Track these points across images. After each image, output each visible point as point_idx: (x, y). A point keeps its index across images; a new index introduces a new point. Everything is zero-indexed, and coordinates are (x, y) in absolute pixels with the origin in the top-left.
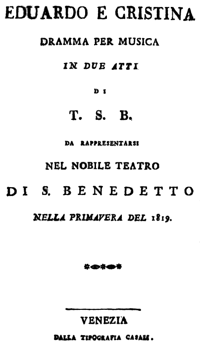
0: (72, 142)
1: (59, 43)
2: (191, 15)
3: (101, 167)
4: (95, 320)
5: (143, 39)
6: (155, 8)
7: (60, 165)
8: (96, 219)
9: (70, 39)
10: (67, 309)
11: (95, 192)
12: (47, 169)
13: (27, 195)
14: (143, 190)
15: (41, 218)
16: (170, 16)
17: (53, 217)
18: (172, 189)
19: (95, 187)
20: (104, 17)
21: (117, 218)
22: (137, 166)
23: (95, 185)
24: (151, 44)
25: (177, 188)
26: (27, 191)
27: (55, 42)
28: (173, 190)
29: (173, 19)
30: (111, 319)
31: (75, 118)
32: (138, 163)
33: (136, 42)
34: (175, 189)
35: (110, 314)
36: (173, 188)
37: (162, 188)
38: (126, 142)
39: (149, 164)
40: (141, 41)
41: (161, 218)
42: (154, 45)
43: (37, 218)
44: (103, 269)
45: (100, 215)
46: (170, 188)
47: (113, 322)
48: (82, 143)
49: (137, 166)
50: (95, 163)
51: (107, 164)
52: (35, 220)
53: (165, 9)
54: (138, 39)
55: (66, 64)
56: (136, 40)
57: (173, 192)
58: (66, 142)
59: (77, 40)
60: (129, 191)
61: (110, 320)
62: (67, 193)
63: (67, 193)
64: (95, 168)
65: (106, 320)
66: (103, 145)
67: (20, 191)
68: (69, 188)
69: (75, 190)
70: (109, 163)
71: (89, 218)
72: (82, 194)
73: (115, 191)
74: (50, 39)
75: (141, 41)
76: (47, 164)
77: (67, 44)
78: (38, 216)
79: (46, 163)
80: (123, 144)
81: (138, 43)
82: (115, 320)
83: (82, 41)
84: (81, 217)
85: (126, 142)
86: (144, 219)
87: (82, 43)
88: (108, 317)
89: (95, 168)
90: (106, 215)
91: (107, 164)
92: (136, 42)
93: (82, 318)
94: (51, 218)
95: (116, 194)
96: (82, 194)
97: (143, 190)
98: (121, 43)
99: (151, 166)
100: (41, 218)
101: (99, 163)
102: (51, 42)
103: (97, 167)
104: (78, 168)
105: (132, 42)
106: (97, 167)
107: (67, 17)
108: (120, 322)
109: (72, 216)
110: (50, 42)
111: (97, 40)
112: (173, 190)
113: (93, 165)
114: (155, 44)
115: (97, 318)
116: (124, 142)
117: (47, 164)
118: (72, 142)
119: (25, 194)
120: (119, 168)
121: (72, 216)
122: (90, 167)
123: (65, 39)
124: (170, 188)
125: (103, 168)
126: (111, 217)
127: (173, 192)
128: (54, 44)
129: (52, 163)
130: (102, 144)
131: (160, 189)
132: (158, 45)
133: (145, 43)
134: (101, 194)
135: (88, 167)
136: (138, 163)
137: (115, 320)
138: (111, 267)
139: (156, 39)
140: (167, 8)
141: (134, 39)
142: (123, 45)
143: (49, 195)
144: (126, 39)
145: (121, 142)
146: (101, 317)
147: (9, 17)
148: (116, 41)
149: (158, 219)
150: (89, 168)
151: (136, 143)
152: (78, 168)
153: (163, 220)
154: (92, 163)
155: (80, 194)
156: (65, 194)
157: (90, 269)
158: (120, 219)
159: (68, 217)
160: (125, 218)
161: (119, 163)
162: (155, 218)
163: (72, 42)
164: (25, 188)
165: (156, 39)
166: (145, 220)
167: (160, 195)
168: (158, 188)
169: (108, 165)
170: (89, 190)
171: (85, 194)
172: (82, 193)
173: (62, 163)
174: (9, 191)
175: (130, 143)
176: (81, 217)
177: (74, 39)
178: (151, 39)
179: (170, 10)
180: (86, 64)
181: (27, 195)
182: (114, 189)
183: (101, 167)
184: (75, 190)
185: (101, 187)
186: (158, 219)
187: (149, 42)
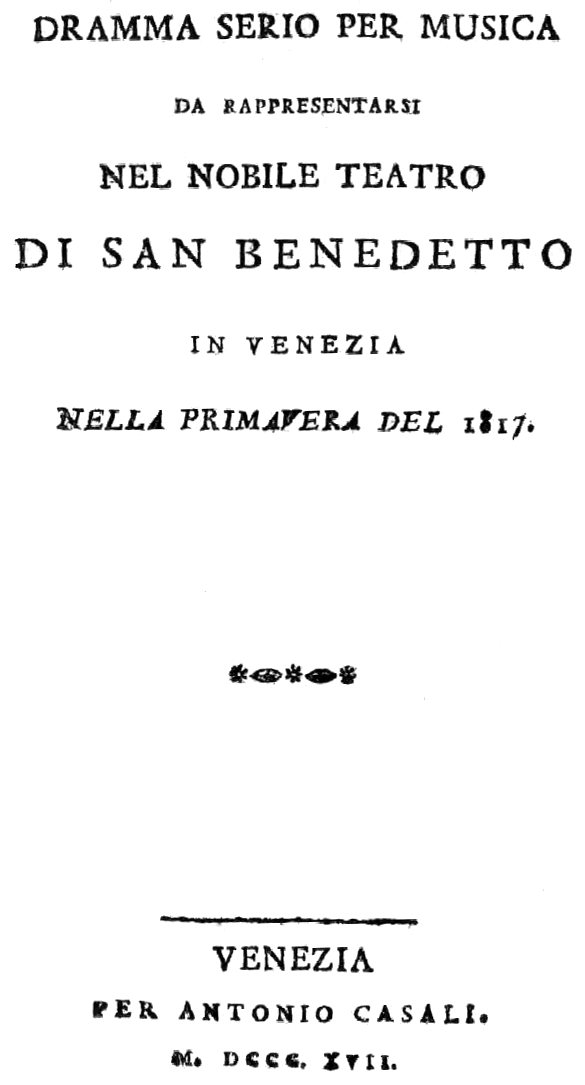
0: (198, 103)
2: (151, 256)
3: (286, 180)
4: (261, 956)
5: (504, 18)
7: (149, 176)
8: (272, 425)
9: (134, 21)
10: (164, 918)
12: (193, 185)
15: (83, 421)
17: (122, 419)
20: (292, 262)
21: (341, 421)
22: (411, 177)
24: (530, 37)
27: (83, 29)
28: (421, 175)
29: (147, 38)
30: (319, 954)
32: (412, 167)
33: (480, 28)
34: (521, 247)
35: (313, 936)
36: (421, 168)
38: (375, 102)
39: (450, 170)
40: (497, 25)
41: (494, 424)
42: (541, 37)
43: (67, 420)
44: (292, 681)
45: (286, 413)
46: (229, 1005)
47: (325, 964)
48: (229, 106)
49: (411, 177)
50: (267, 167)
52: (62, 426)
54: (492, 37)
55: (469, 420)
56: (479, 21)
57: (516, 255)
58: (227, 1055)
61: (312, 959)
62: (250, 260)
64: (268, 185)
65: (299, 959)
66: (300, 111)
71: (249, 420)
75: (497, 25)
78: (73, 415)
80: (366, 107)
81: (488, 34)
82: (332, 958)
83: (175, 27)
84: (220, 420)
85: (375, 102)
86: (435, 425)
88: (306, 949)
89: (268, 185)
90: (307, 414)
92: (480, 28)
93: (218, 950)
94: (115, 424)
98: (430, 32)
99: (456, 178)
100: (83, 421)
101: (281, 166)
102: (69, 27)
103: (273, 180)
104: (208, 184)
105: (466, 28)
106: (273, 180)
107: (394, 266)
108: (348, 965)
109: (189, 415)
111: (348, 22)
112: (421, 175)
113: (262, 174)
114: (547, 33)
115: (267, 949)
116: (370, 102)
118: (198, 103)
120: (348, 184)
121: (189, 415)
122: (252, 181)
123: (118, 19)
124: (338, 167)
125: (292, 184)
126: (322, 421)
127: (516, 255)
129: (120, 168)
130: (295, 106)
131: (521, 247)
132: (554, 37)
133: (509, 32)
135: (241, 181)
136: (412, 167)
137: (332, 958)
138: (321, 676)
139: (548, 20)
141: (474, 17)
142: (435, 41)
143: (484, 1019)
144: (444, 18)
145: (359, 101)
146: (282, 949)
147: (365, 263)
148: (409, 25)
149: (485, 428)
150: (246, 185)
151: (412, 106)
152: (208, 184)
153: (502, 431)
154: (256, 169)
156: (242, 265)
157: (249, 681)
158: (353, 424)
159: (173, 420)
160: (370, 421)
161: (348, 168)
162: (477, 423)
163: (141, 32)
165: (548, 20)
166: (438, 430)
167: (61, 240)
173: (156, 168)
174: (361, 258)
175: (390, 105)
176: (220, 420)
177: (150, 19)
178: (531, 18)
180: (386, 415)
182: (311, 417)
183: (286, 180)
186: (485, 428)
187: (524, 27)
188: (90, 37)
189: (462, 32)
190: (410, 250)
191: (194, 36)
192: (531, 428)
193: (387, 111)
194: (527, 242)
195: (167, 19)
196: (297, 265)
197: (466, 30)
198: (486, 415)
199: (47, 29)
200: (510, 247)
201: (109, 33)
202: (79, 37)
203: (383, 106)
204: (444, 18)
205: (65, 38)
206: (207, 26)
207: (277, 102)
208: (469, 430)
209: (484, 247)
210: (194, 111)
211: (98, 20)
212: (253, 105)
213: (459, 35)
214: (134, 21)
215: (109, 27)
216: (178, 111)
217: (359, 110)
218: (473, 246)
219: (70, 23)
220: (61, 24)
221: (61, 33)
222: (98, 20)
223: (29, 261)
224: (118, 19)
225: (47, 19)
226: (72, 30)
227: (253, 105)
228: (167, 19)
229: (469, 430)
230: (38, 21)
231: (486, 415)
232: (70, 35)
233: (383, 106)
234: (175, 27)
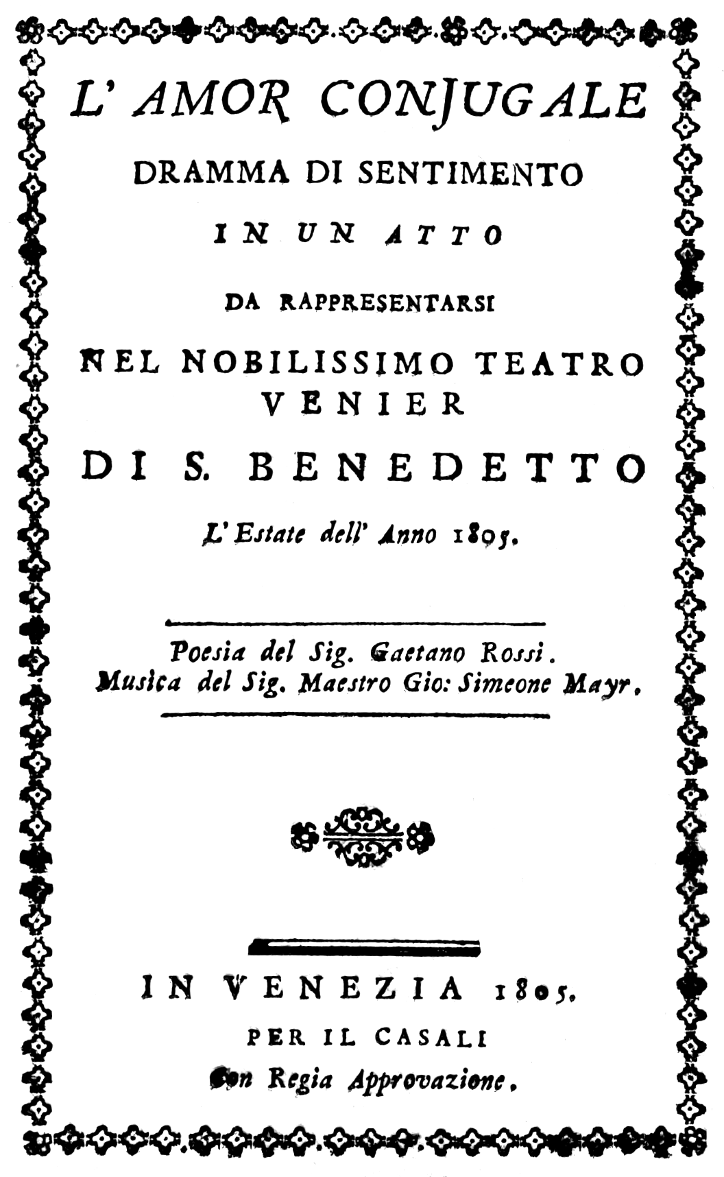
1: (193, 176)
6: (425, 164)
9: (228, 164)
11: (342, 470)
12: (186, 370)
13: (544, 480)
14: (492, 462)
16: (458, 177)
18: (533, 460)
19: (343, 457)
20: (278, 993)
23: (341, 452)
25: (595, 457)
26: (143, 465)
27: (180, 173)
31: (571, 111)
37: (550, 457)
46: (574, 457)
48: (181, 985)
51: (312, 397)
53: (448, 168)
59: (473, 171)
60: (448, 467)
62: (262, 472)
63: (262, 472)
67: (124, 465)
68: (268, 457)
69: (284, 466)
70: (317, 394)
72: (496, 479)
73: (276, 987)
74: (163, 163)
76: (187, 354)
77: (219, 179)
79: (185, 351)
80: (437, 305)
83: (268, 170)
87: (266, 176)
91: (312, 397)
95: (408, 478)
96: (496, 479)
97: (492, 462)
102: (167, 172)
110: (164, 173)
116: (442, 300)
117: (187, 354)
118: (252, 299)
119: (138, 476)
123: (212, 164)
128: (177, 181)
131: (545, 460)
134: (361, 477)
140: (453, 164)
144: (482, 165)
155: (487, 478)
156: (254, 477)
162: (466, 533)
163: (235, 176)
164: (147, 994)
167: (589, 480)
168: (539, 457)
169: (314, 402)
170: (327, 466)
171: (503, 478)
172: (495, 473)
174: (394, 472)
177: (243, 164)
179: (459, 168)
181: (544, 480)
182: (368, 299)
184: (284, 466)
185: (189, 978)
186: (473, 539)
188: (187, 180)
189: (473, 106)
190: (453, 461)
191: (284, 180)
192: (515, 541)
193: (460, 310)
194: (351, 86)
195: (259, 165)
196: (315, 477)
197: (478, 103)
198: (474, 526)
199: (146, 172)
200: (429, 167)
201: (205, 177)
202: (177, 181)
203: (455, 303)
204: (482, 165)
205: (163, 181)
206: (296, 171)
207: (337, 297)
208: (458, 540)
209: (438, 167)
210: (247, 307)
211: (194, 164)
212: (313, 301)
213: (468, 108)
214: (228, 164)
215: (204, 170)
216: (229, 307)
217: (430, 309)
218: (579, 460)
219: (168, 168)
220: (159, 167)
221: (159, 176)
222: (194, 164)
223: (260, 476)
224: (212, 164)
225: (410, 690)
226: (169, 174)
227: (313, 301)
228: (259, 165)
229: (458, 540)
230: (138, 164)
231: (474, 526)
232: (167, 178)
233: (455, 303)
234: (268, 170)
